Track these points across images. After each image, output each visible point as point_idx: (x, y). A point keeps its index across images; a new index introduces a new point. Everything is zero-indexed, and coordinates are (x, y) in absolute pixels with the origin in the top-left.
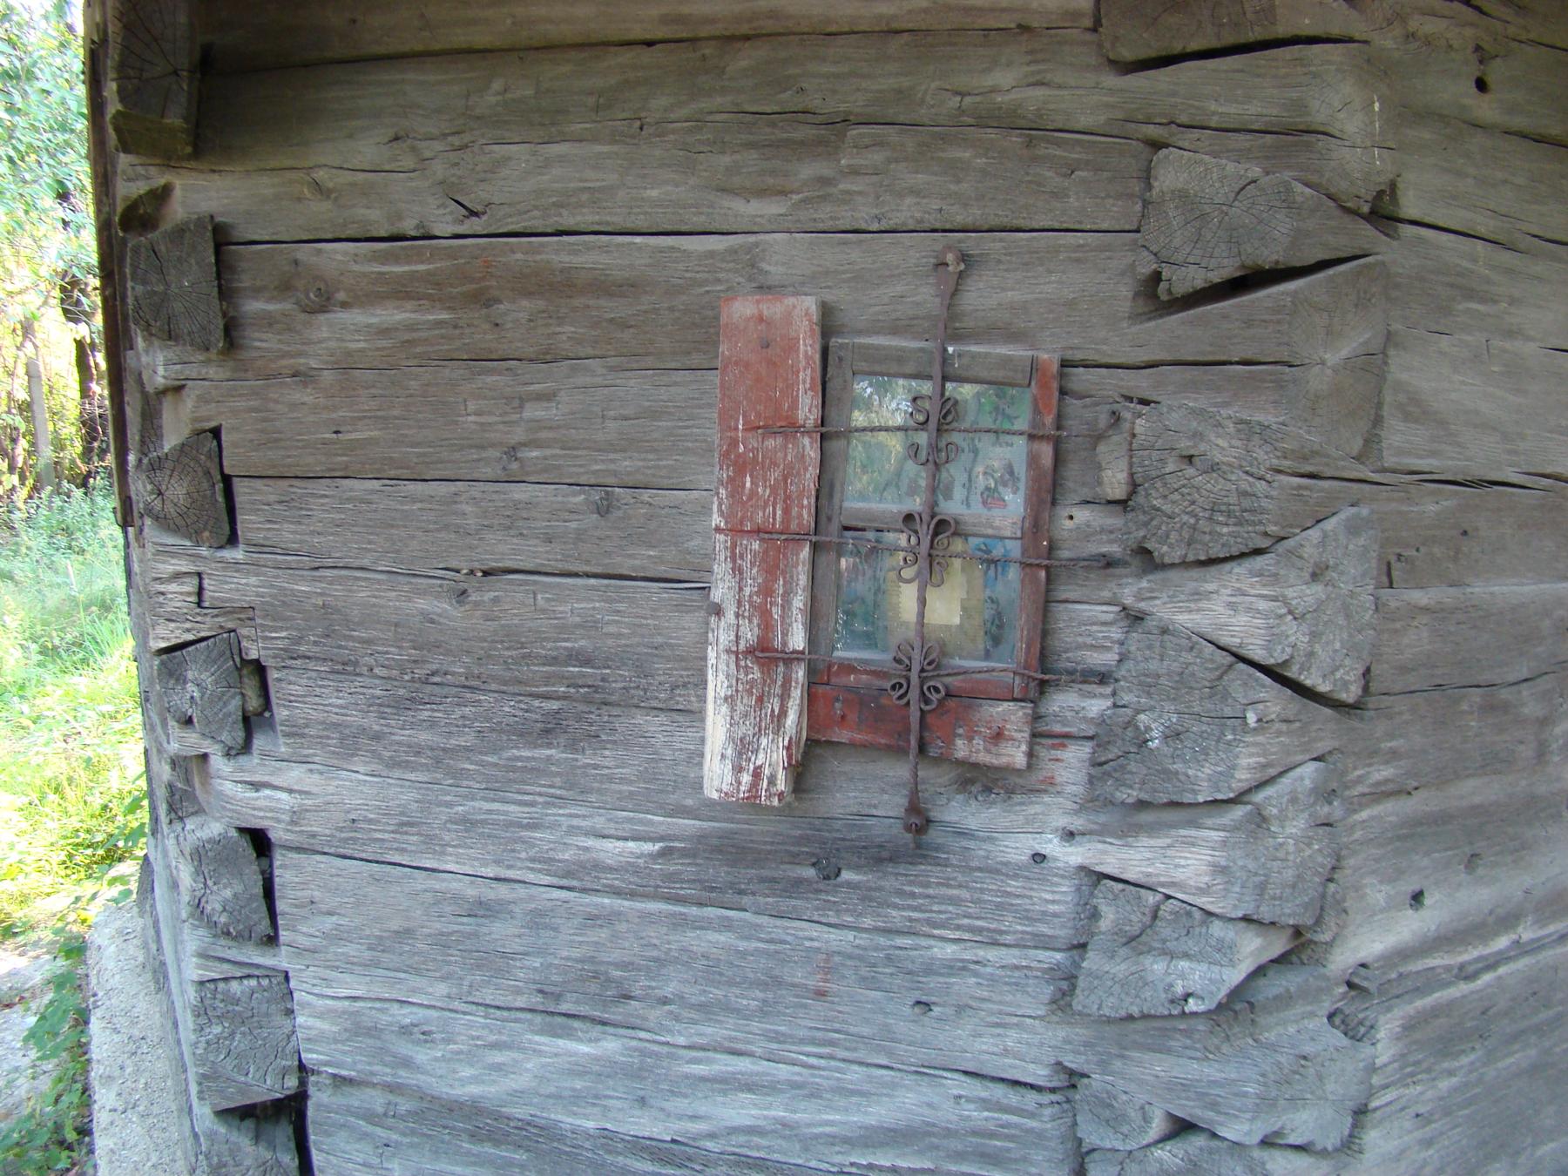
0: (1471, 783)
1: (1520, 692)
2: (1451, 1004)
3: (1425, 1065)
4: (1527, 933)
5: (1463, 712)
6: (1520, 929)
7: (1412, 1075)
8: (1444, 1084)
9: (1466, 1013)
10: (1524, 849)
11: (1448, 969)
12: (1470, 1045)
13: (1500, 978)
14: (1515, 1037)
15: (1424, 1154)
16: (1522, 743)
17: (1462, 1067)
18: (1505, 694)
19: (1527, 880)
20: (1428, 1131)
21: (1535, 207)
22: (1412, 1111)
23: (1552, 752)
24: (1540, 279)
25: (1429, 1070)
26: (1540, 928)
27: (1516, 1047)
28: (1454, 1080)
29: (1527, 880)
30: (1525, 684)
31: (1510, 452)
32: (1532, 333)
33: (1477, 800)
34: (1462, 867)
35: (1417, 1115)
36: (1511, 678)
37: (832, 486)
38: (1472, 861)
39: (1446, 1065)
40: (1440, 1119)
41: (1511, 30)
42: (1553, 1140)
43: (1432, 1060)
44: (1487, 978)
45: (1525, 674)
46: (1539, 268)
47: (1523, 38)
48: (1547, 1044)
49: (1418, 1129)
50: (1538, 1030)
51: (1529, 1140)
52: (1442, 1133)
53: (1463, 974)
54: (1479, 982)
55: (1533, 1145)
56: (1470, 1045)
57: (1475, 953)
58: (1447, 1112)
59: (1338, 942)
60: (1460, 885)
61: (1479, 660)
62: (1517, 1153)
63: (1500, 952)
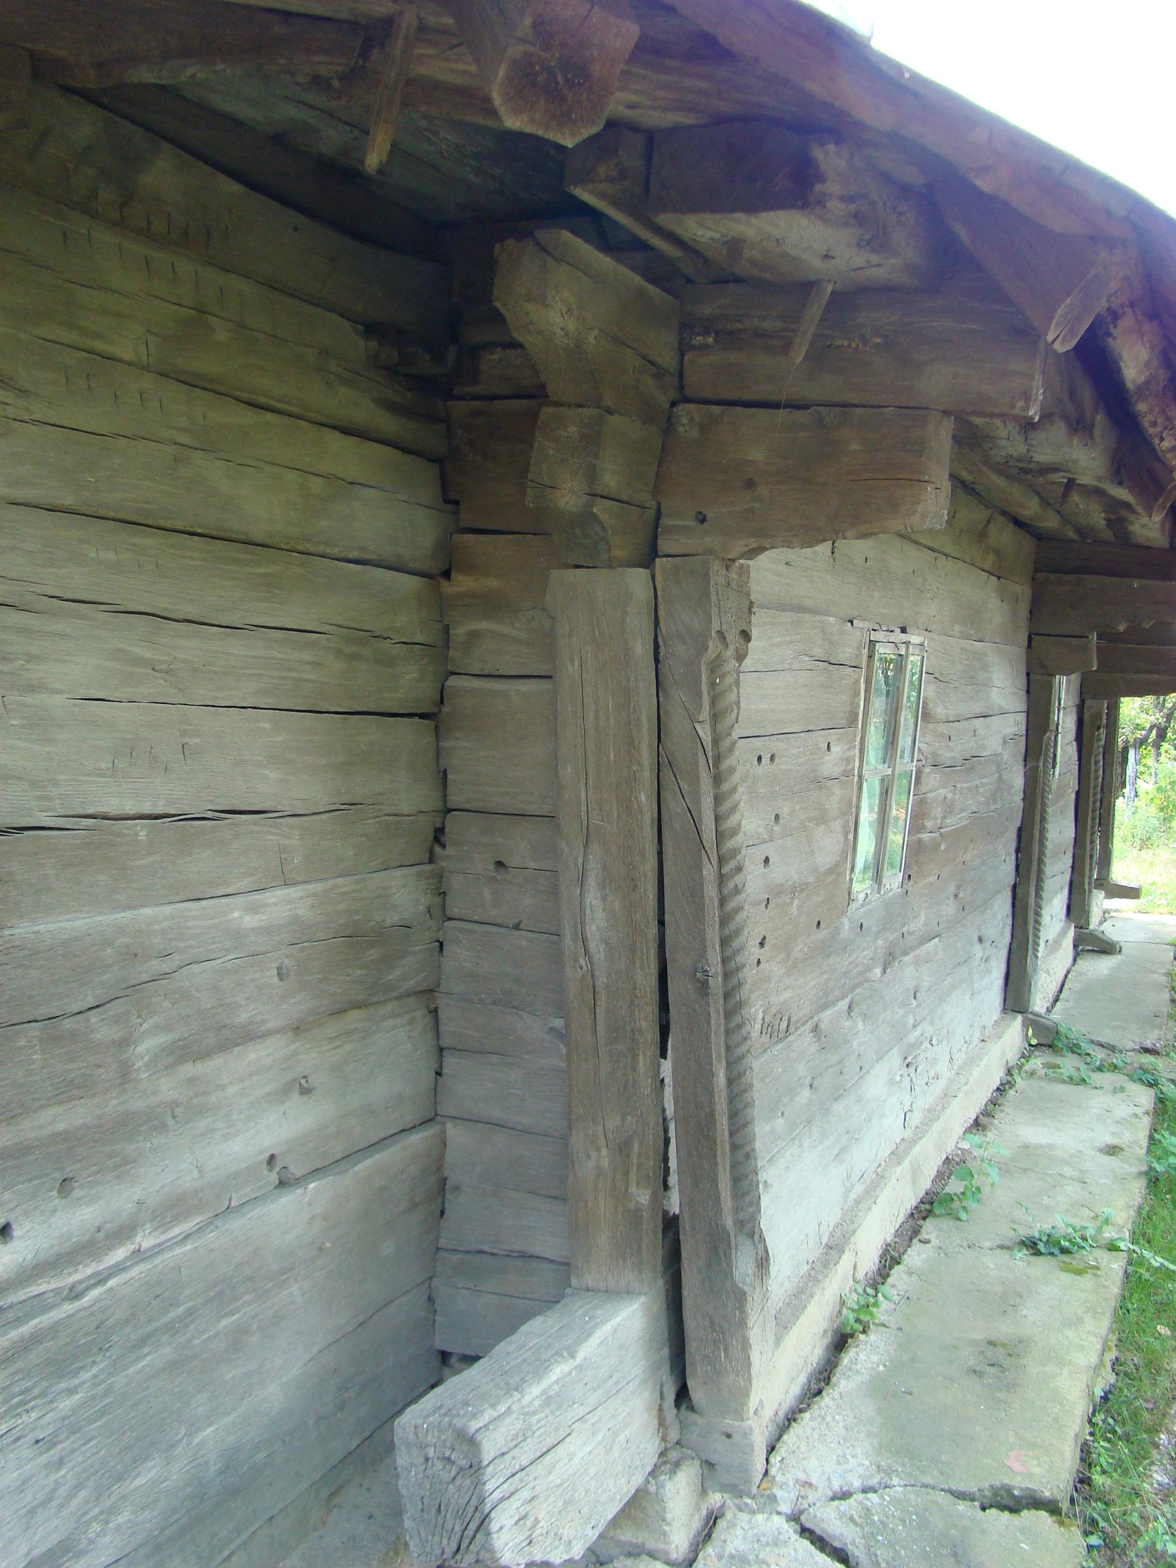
0: (48, 1114)
1: (87, 1020)
2: (55, 1329)
3: (36, 1391)
4: (146, 1240)
5: (20, 1048)
6: (138, 1239)
7: (22, 1403)
8: (66, 1404)
9: (77, 1332)
10: (127, 1163)
11: (57, 1292)
12: (91, 1360)
13: (111, 1289)
14: (143, 1341)
15: (53, 1477)
16: (99, 1066)
17: (83, 1383)
18: (67, 1024)
19: (137, 1192)
20: (54, 1453)
21: (51, 570)
22: (30, 1438)
23: (138, 1070)
24: (61, 636)
25: (42, 1395)
26: (163, 1233)
27: (146, 1350)
28: (76, 1397)
29: (137, 1192)
30: (93, 1012)
31: (41, 798)
32: (57, 686)
33: (60, 1127)
34: (55, 1192)
35: (37, 1442)
36: (75, 1008)
37: (889, 730)
38: (65, 1186)
39: (64, 1385)
40: (67, 1438)
41: (11, 412)
42: (210, 1425)
43: (45, 1384)
44: (95, 1293)
45: (91, 1001)
46: (60, 626)
47: (27, 418)
48: (183, 1339)
49: (40, 1454)
50: (170, 1328)
51: (183, 1431)
52: (73, 1452)
53: (74, 1294)
54: (86, 1299)
55: (190, 1435)
56: (91, 1360)
57: (89, 1271)
58: (75, 1430)
59: (940, 1219)
60: (55, 1211)
61: (30, 997)
62: (172, 1447)
63: (118, 1264)
